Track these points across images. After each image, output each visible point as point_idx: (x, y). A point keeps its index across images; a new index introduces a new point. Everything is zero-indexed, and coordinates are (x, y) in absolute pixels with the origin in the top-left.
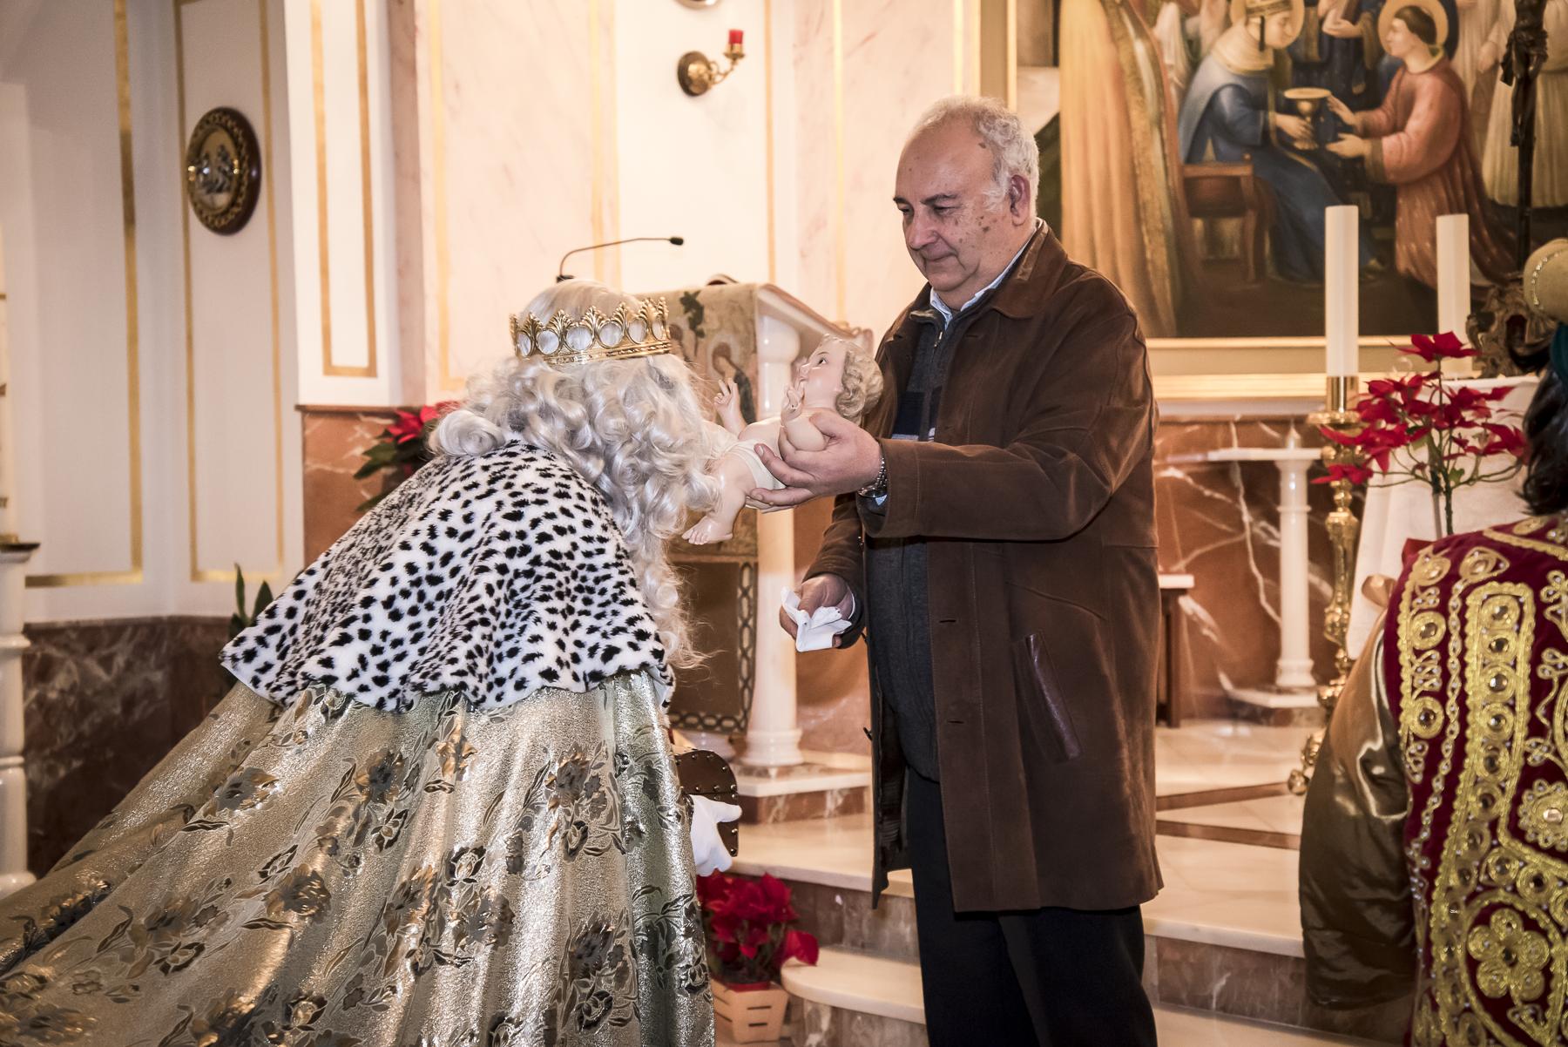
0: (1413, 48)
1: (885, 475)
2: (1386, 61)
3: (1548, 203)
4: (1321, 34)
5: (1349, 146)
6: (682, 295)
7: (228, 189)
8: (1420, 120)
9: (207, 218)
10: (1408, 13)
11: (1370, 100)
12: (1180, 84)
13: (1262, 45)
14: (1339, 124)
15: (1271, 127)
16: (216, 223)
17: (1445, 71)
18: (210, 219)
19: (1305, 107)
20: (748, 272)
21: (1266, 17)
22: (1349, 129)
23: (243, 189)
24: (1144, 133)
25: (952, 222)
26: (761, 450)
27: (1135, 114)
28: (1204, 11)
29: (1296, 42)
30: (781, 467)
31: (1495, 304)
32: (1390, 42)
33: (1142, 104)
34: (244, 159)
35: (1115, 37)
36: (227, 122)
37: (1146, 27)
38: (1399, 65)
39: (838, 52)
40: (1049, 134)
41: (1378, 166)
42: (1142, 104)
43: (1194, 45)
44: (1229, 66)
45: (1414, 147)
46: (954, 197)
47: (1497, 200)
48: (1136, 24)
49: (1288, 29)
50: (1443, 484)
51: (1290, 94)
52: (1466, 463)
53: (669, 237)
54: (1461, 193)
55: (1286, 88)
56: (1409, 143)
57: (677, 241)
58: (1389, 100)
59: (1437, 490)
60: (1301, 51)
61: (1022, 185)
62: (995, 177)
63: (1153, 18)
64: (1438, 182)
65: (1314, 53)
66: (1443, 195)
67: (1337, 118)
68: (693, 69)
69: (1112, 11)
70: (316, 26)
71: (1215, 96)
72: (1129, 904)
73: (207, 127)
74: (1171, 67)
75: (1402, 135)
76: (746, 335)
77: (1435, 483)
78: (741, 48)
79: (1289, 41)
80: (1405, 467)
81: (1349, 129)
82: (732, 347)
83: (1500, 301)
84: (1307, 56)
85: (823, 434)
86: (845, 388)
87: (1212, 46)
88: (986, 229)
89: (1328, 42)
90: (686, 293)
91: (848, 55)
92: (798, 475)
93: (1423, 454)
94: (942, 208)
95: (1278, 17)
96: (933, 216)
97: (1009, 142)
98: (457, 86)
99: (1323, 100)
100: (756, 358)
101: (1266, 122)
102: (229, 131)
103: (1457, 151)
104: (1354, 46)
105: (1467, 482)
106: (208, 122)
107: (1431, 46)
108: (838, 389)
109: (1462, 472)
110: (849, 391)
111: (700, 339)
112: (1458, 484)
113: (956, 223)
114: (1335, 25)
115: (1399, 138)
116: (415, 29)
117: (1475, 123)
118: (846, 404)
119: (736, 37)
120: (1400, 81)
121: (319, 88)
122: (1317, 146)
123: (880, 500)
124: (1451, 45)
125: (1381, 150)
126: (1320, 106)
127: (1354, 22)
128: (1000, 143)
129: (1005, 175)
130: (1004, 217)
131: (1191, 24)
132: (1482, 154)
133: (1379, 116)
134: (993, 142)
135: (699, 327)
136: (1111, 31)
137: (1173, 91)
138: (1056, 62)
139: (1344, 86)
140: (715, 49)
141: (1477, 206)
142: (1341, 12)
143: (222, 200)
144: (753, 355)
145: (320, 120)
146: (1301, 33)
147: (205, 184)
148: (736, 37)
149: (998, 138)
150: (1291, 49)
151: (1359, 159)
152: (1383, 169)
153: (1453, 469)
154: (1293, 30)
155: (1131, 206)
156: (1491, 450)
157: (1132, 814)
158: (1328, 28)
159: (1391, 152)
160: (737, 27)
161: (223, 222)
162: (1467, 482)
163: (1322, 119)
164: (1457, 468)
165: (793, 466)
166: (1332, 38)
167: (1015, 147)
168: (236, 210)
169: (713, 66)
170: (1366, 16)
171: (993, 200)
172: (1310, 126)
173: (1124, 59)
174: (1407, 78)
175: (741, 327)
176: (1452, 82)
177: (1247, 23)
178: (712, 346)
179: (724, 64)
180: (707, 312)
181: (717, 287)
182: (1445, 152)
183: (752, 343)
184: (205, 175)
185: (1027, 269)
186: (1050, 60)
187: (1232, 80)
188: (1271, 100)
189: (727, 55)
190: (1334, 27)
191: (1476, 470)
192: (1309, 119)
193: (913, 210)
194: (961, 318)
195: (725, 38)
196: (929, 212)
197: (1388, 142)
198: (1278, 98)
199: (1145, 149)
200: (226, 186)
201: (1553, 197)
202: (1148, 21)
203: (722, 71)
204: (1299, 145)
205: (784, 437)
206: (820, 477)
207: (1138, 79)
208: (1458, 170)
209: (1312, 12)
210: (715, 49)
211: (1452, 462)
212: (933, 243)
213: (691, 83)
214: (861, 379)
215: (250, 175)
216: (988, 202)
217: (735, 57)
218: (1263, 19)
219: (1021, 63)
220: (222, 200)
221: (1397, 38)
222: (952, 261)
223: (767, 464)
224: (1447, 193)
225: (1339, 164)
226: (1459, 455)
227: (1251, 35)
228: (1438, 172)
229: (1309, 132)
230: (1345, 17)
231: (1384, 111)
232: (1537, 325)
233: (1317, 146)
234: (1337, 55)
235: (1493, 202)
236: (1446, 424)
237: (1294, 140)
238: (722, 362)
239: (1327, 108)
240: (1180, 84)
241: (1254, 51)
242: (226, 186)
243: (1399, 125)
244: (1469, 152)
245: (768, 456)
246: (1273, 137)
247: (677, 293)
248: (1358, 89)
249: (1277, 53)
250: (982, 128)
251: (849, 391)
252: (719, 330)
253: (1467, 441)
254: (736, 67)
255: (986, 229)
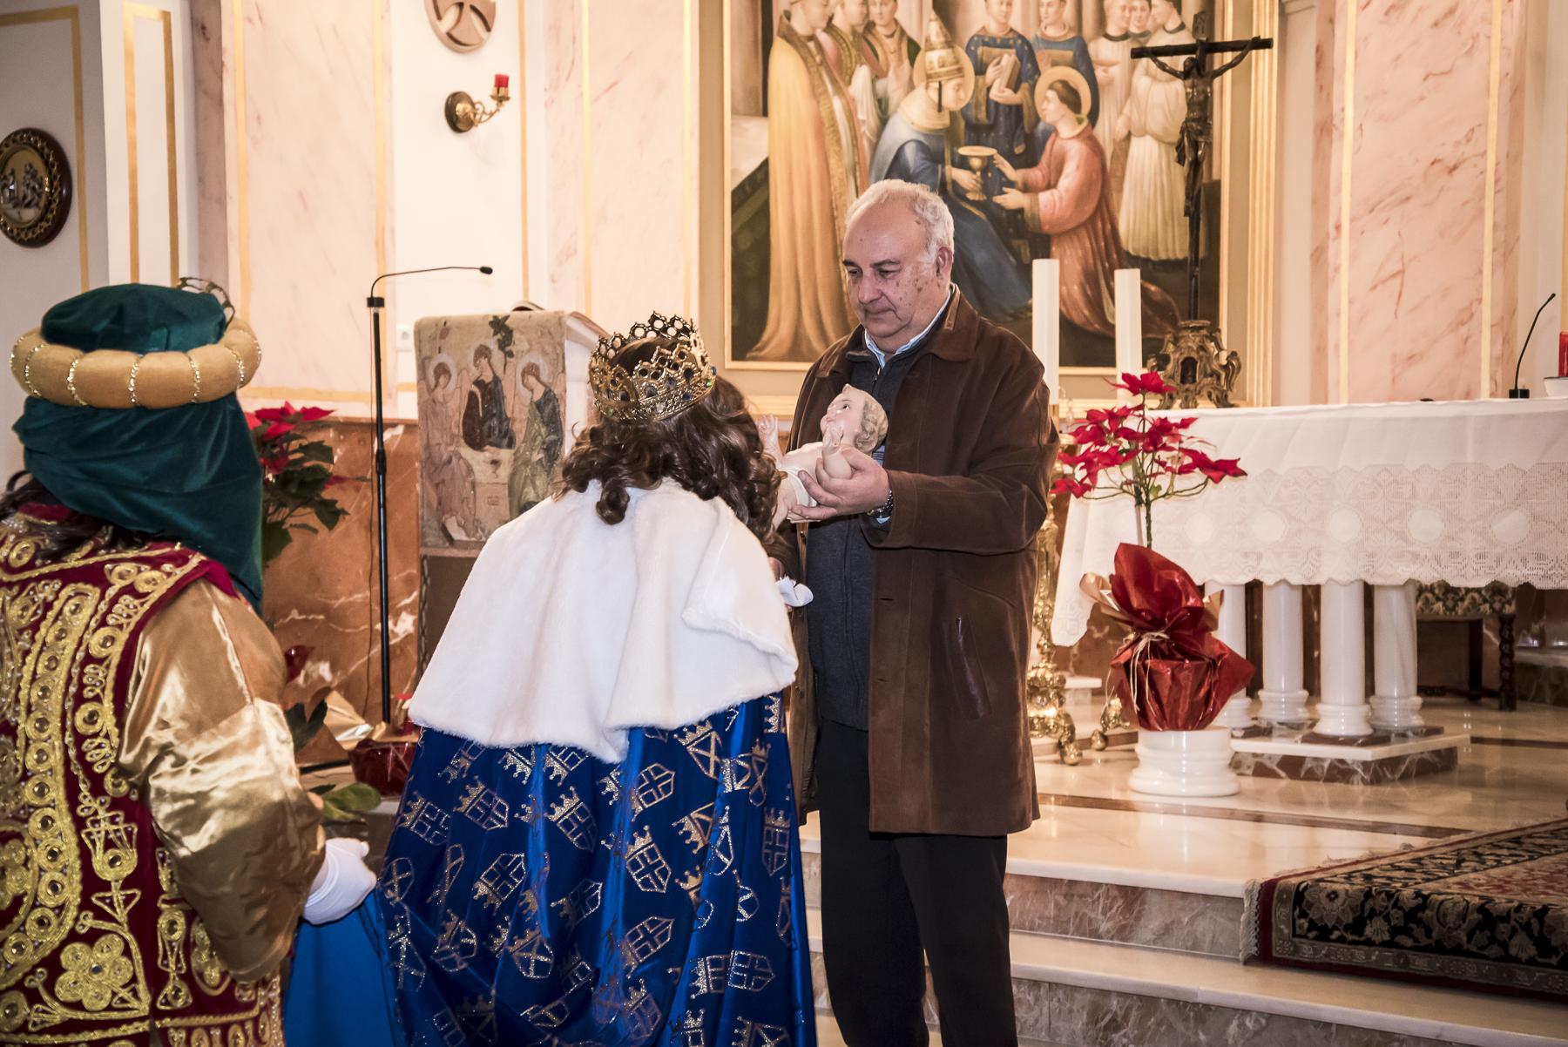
0: (1063, 116)
1: (891, 501)
2: (1041, 126)
3: (1171, 256)
4: (988, 100)
5: (1012, 199)
6: (491, 319)
7: (37, 205)
8: (1070, 178)
9: (12, 231)
10: (1059, 86)
11: (1028, 160)
12: (871, 138)
13: (940, 108)
14: (1004, 179)
15: (948, 180)
16: (23, 236)
17: (1089, 138)
18: (15, 232)
19: (976, 163)
20: (548, 301)
21: (943, 83)
22: (1011, 184)
23: (54, 206)
24: (841, 180)
25: (895, 284)
26: (803, 475)
27: (833, 162)
28: (891, 73)
29: (968, 105)
30: (817, 489)
31: (1171, 347)
32: (1043, 110)
33: (839, 152)
34: (55, 177)
35: (816, 93)
36: (36, 142)
37: (842, 84)
38: (1051, 131)
39: (587, 99)
40: (759, 177)
41: (1036, 218)
42: (840, 159)
43: (883, 103)
44: (912, 123)
45: (1064, 203)
46: (896, 263)
47: (1131, 251)
48: (834, 82)
49: (962, 94)
50: (1144, 497)
51: (963, 151)
52: (1163, 481)
53: (480, 266)
54: (1103, 244)
55: (959, 146)
56: (1061, 198)
57: (487, 271)
58: (1044, 160)
59: (1139, 502)
60: (972, 113)
61: (946, 254)
62: (927, 247)
63: (847, 78)
64: (1083, 233)
65: (982, 116)
66: (1088, 245)
67: (1002, 174)
68: (460, 108)
69: (813, 70)
70: (129, 57)
71: (901, 149)
72: (1001, 834)
73: (12, 145)
74: (864, 122)
75: (1054, 191)
76: (555, 357)
77: (1138, 495)
78: (507, 92)
79: (962, 105)
80: (1115, 483)
81: (1011, 184)
82: (541, 367)
83: (1175, 344)
84: (977, 119)
85: (852, 466)
86: (864, 429)
87: (898, 106)
88: (920, 290)
89: (994, 107)
90: (495, 317)
91: (595, 100)
92: (830, 497)
93: (1128, 472)
94: (887, 272)
95: (954, 83)
96: (879, 278)
97: (937, 220)
98: (259, 118)
99: (991, 158)
100: (565, 377)
101: (943, 174)
102: (40, 152)
103: (1099, 208)
104: (1016, 112)
105: (1164, 496)
106: (14, 141)
107: (1079, 116)
108: (857, 430)
109: (1159, 488)
110: (867, 433)
111: (508, 359)
112: (1157, 498)
113: (898, 284)
114: (1001, 93)
115: (1052, 194)
116: (222, 64)
117: (1113, 183)
118: (863, 443)
119: (501, 82)
120: (1053, 144)
121: (131, 114)
122: (985, 198)
123: (882, 520)
124: (1094, 116)
125: (1038, 204)
126: (988, 163)
127: (1015, 91)
128: (931, 221)
129: (934, 247)
130: (932, 281)
131: (881, 84)
132: (1119, 211)
133: (1036, 174)
134: (926, 220)
135: (508, 349)
136: (813, 87)
137: (866, 144)
138: (765, 113)
139: (1007, 146)
140: (482, 92)
141: (1115, 256)
142: (1004, 83)
143: (30, 214)
144: (561, 375)
145: (132, 144)
146: (972, 98)
147: (11, 199)
148: (501, 82)
149: (929, 216)
150: (964, 111)
151: (1021, 211)
152: (1039, 219)
153: (1153, 486)
154: (966, 94)
155: (830, 246)
156: (1184, 470)
157: (1021, 761)
158: (994, 95)
159: (1046, 206)
160: (503, 72)
161: (30, 235)
162: (1164, 496)
163: (990, 175)
164: (1156, 485)
165: (827, 490)
166: (997, 104)
167: (941, 223)
168: (44, 224)
169: (477, 106)
170: (1025, 86)
171: (926, 266)
172: (979, 179)
173: (824, 113)
174: (1058, 142)
175: (548, 348)
176: (1096, 148)
177: (927, 87)
178: (522, 365)
179: (491, 105)
180: (516, 335)
181: (526, 313)
182: (1090, 208)
183: (560, 364)
184: (11, 191)
185: (949, 324)
186: (761, 112)
187: (914, 136)
188: (947, 155)
189: (493, 97)
190: (1000, 95)
191: (1172, 485)
192: (979, 173)
193: (862, 272)
194: (896, 362)
195: (492, 82)
196: (875, 275)
197: (1044, 197)
198: (953, 154)
199: (841, 195)
200: (34, 202)
201: (1174, 251)
202: (844, 80)
203: (488, 111)
204: (970, 196)
205: (820, 467)
206: (845, 500)
207: (836, 132)
208: (1100, 225)
209: (980, 78)
210: (482, 92)
211: (1152, 479)
212: (877, 299)
213: (457, 118)
214: (876, 423)
215: (61, 192)
216: (922, 268)
217: (501, 99)
218: (940, 83)
219: (734, 112)
220: (30, 214)
221: (1050, 108)
222: (890, 315)
223: (807, 487)
224: (1091, 244)
225: (1004, 215)
226: (1161, 473)
227: (932, 100)
228: (1084, 225)
229: (979, 185)
230: (1008, 86)
231: (1040, 170)
232: (1205, 365)
233: (985, 198)
234: (1001, 119)
235: (1128, 253)
236: (1151, 448)
237: (967, 191)
238: (532, 380)
239: (994, 165)
240: (871, 138)
241: (934, 111)
242: (34, 202)
243: (1052, 183)
244: (1108, 207)
245: (809, 480)
246: (949, 188)
247: (486, 317)
248: (1019, 150)
249: (952, 114)
250: (917, 209)
251: (867, 433)
252: (529, 351)
253: (1165, 463)
254: (501, 109)
255: (920, 290)
